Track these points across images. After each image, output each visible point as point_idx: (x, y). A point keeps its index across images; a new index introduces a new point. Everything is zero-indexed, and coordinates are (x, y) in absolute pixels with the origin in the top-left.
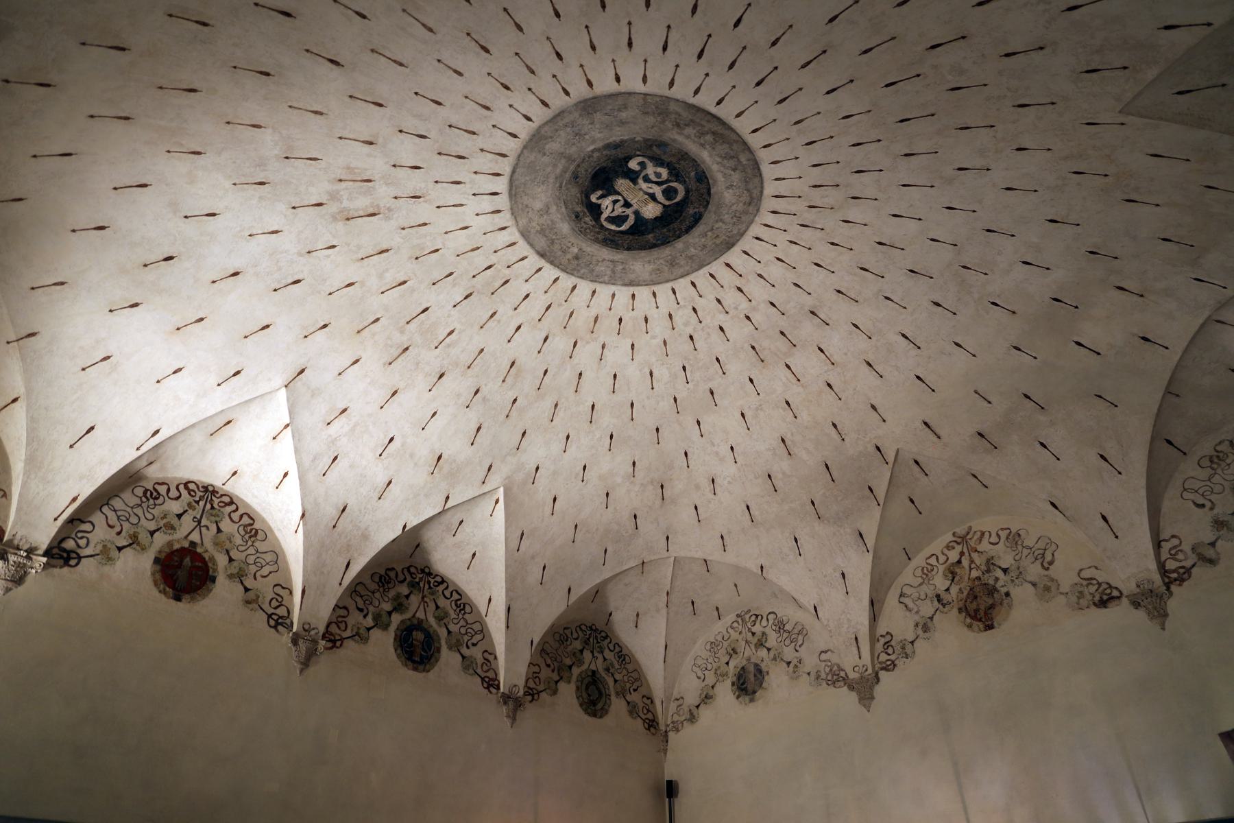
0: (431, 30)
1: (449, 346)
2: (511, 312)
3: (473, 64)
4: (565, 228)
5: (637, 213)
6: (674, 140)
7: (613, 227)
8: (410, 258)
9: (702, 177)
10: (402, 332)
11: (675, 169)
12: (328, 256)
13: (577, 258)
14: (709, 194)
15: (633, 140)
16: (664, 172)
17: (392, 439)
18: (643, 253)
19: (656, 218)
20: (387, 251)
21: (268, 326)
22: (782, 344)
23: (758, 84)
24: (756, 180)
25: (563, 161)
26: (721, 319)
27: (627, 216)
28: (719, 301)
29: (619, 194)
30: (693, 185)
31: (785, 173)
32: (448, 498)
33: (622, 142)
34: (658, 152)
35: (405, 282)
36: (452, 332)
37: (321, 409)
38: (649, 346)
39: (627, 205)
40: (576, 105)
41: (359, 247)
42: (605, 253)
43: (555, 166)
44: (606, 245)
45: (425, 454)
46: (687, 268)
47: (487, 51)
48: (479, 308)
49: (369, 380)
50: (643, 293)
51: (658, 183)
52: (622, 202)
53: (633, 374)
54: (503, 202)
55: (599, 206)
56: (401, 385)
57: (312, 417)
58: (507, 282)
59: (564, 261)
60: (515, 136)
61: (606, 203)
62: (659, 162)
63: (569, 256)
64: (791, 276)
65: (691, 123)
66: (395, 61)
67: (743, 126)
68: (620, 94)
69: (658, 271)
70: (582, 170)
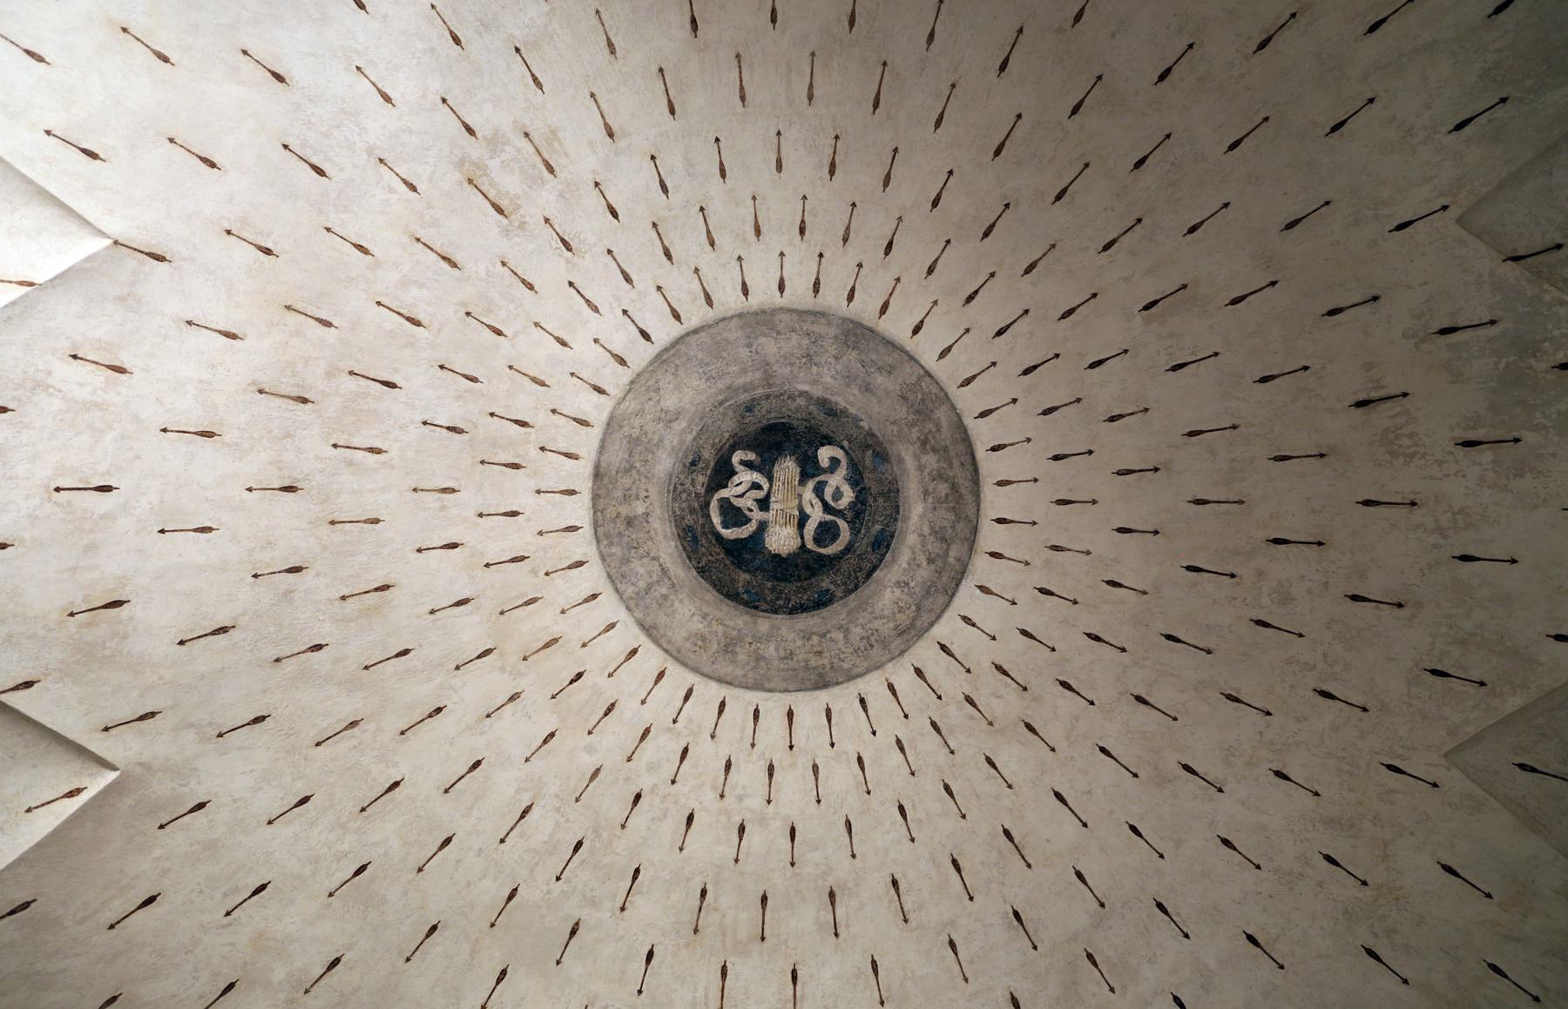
0: (810, 97)
1: (351, 463)
2: (471, 513)
3: (804, 168)
4: (664, 464)
5: (763, 526)
6: (901, 460)
7: (716, 520)
8: (463, 304)
9: (883, 544)
10: (330, 375)
11: (863, 503)
12: (391, 190)
13: (630, 522)
14: (869, 575)
15: (857, 420)
16: (848, 495)
17: (106, 489)
18: (711, 595)
19: (777, 556)
20: (454, 265)
21: (213, 165)
22: (748, 918)
23: (1056, 458)
24: (942, 599)
25: (759, 375)
26: (704, 802)
27: (748, 520)
28: (728, 766)
29: (770, 479)
30: (862, 545)
31: (986, 616)
32: (28, 685)
33: (844, 412)
34: (868, 463)
35: (417, 323)
36: (378, 451)
37: (97, 327)
38: (572, 753)
39: (764, 504)
40: (845, 320)
41: (435, 224)
42: (667, 549)
43: (744, 371)
44: (681, 538)
45: (106, 574)
46: (739, 672)
47: (832, 172)
48: (445, 461)
49: (206, 376)
50: (651, 658)
51: (827, 508)
52: (761, 494)
53: (504, 786)
54: (641, 354)
55: (734, 473)
56: (230, 436)
57: (71, 320)
58: (516, 466)
59: (611, 512)
60: (745, 292)
61: (746, 477)
62: (855, 480)
63: (624, 510)
64: (853, 804)
65: (941, 451)
66: (742, 88)
67: (995, 502)
68: (902, 350)
69: (702, 640)
70: (765, 405)
